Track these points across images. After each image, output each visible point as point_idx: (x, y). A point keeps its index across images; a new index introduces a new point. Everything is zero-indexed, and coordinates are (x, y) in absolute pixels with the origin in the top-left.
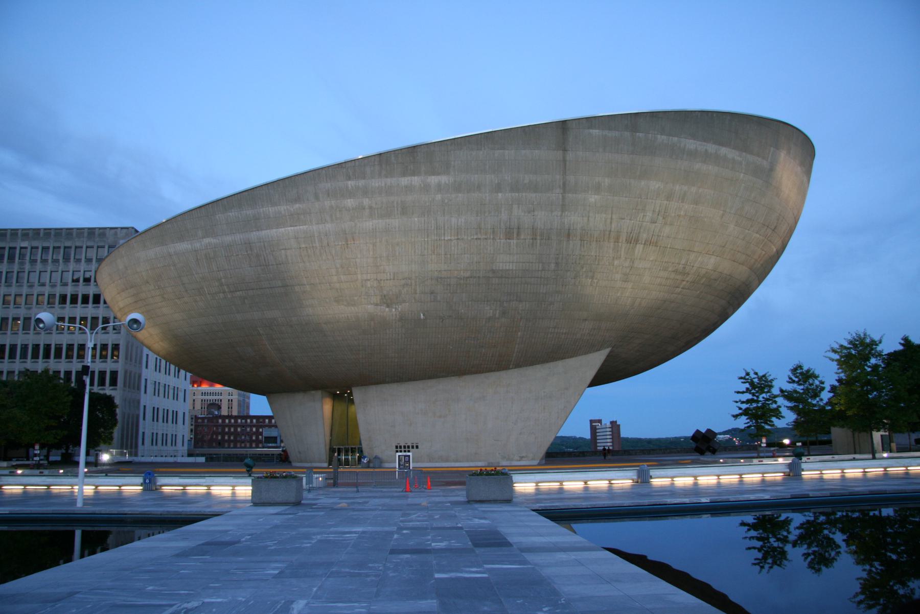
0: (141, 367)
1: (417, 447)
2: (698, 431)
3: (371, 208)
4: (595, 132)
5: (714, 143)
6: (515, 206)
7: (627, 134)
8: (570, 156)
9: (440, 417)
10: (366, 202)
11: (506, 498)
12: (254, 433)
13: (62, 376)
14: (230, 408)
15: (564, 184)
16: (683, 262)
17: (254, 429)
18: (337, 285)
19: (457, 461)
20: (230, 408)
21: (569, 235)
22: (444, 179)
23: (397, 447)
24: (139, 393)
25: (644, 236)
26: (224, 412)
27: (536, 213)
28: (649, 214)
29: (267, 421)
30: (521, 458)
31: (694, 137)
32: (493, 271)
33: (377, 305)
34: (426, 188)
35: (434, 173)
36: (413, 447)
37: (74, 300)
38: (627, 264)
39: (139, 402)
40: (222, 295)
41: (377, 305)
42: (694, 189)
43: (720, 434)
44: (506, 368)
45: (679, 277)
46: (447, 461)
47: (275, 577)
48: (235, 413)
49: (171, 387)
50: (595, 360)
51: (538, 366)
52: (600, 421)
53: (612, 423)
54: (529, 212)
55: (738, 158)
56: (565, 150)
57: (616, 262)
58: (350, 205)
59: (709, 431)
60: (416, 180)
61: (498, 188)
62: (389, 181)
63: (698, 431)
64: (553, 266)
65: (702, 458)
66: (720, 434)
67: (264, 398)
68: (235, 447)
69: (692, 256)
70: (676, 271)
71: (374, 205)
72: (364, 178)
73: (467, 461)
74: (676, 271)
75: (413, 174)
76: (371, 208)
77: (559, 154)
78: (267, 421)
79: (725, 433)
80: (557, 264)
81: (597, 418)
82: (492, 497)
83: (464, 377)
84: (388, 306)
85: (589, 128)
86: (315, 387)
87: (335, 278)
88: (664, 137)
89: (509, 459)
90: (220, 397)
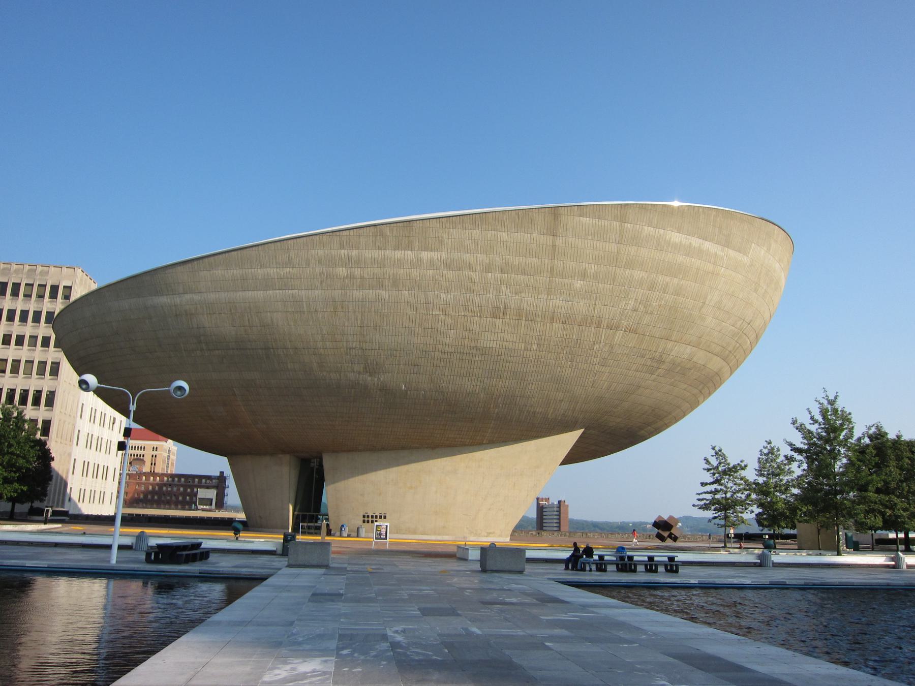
0: (75, 418)
1: (385, 517)
2: (53, 459)
3: (362, 278)
4: (585, 220)
7: (616, 224)
8: (560, 241)
9: (411, 488)
10: (358, 272)
11: (518, 569)
12: (181, 494)
13: (40, 425)
14: (153, 464)
15: (552, 269)
16: (660, 350)
17: (182, 489)
18: (322, 352)
19: (424, 533)
20: (153, 464)
21: (552, 318)
22: (436, 255)
23: (364, 516)
24: (71, 445)
26: (146, 469)
27: (523, 294)
28: (632, 303)
29: (176, 479)
30: (489, 534)
31: (679, 231)
33: (359, 373)
34: (418, 263)
35: (427, 249)
36: (381, 517)
37: (20, 341)
38: (606, 349)
39: (70, 455)
42: (676, 281)
45: (655, 365)
46: (415, 533)
48: (159, 470)
49: (95, 438)
50: (570, 438)
52: (547, 500)
53: (559, 502)
55: (720, 253)
58: (341, 273)
59: (671, 517)
60: (409, 255)
61: (488, 268)
62: (382, 252)
63: (53, 459)
69: (670, 345)
71: (366, 276)
72: (358, 248)
73: (435, 534)
74: (652, 359)
75: (407, 248)
77: (549, 239)
78: (176, 479)
81: (544, 497)
82: (507, 568)
84: (371, 375)
86: (284, 452)
87: (320, 345)
89: (476, 535)
90: (142, 452)
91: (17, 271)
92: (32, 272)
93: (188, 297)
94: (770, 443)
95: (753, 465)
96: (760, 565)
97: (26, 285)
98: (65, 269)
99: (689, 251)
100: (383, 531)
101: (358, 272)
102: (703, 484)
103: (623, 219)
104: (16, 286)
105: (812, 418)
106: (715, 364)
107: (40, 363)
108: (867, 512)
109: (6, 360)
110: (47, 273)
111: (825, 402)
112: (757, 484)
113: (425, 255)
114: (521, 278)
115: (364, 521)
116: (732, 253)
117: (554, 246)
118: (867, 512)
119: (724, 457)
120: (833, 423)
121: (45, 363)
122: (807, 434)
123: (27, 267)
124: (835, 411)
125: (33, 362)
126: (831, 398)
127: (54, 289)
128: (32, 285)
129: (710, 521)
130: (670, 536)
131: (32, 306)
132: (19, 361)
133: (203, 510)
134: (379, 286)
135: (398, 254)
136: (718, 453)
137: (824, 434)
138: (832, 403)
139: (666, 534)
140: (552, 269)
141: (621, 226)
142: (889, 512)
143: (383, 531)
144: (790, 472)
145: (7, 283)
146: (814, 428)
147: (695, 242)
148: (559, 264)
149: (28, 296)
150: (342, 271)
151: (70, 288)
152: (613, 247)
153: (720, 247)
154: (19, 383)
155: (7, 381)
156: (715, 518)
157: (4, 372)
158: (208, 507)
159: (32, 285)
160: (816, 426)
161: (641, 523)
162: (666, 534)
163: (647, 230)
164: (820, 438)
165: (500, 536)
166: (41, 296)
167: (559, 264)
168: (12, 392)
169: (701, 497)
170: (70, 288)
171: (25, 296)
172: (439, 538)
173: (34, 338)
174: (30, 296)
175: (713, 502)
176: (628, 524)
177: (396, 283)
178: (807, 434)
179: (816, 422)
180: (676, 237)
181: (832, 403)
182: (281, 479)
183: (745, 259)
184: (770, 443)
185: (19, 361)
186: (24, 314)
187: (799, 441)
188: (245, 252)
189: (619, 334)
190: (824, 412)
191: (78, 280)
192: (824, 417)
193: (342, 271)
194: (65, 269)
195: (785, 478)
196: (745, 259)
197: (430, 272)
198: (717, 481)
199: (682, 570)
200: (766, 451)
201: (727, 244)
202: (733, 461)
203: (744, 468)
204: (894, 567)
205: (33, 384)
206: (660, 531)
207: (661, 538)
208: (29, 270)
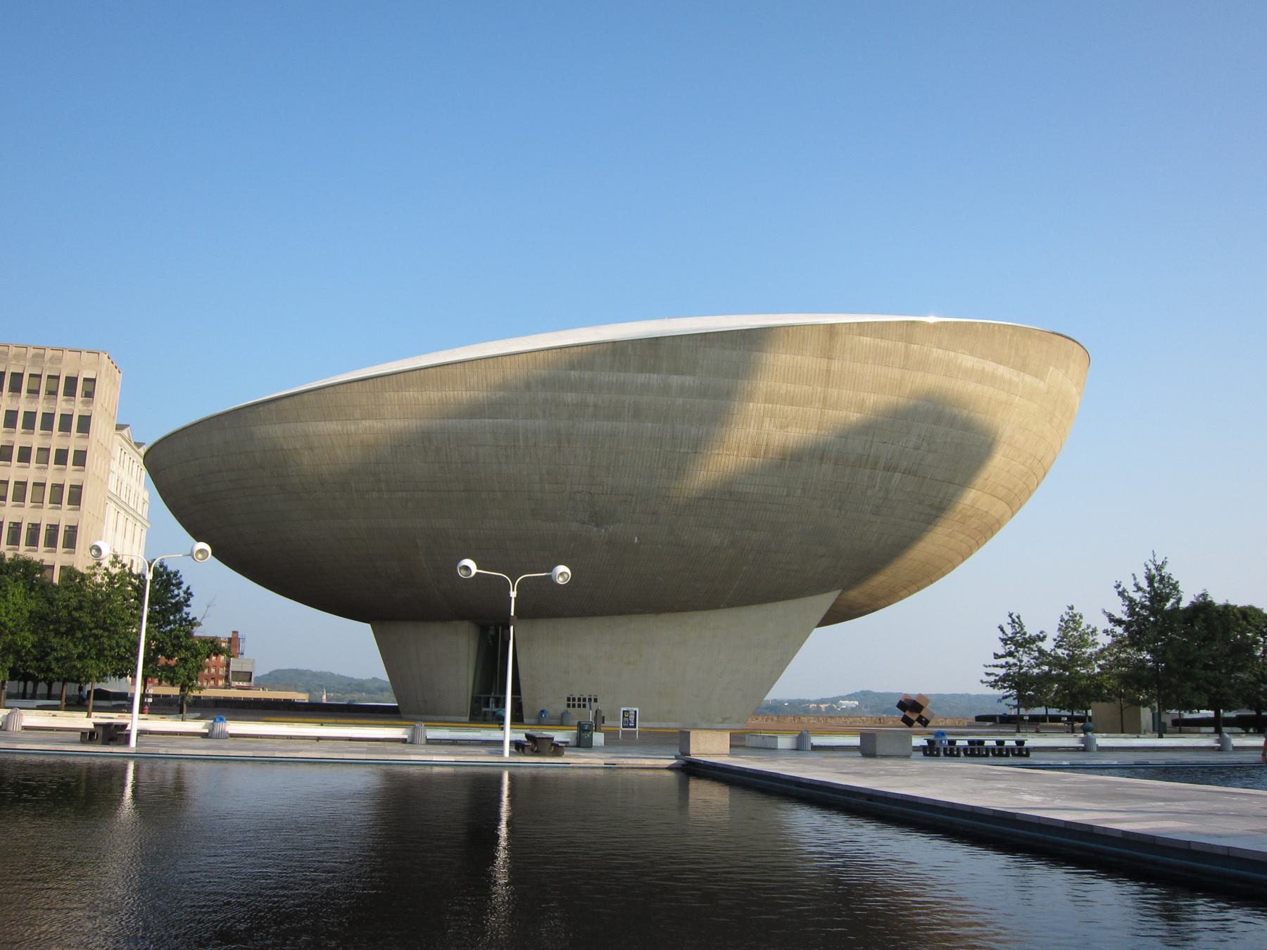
1: (596, 700)
3: (595, 406)
4: (866, 340)
5: (993, 361)
6: (767, 420)
7: (901, 345)
8: (836, 365)
10: (591, 398)
15: (825, 398)
21: (822, 459)
22: (688, 380)
23: (569, 699)
25: (904, 464)
31: (972, 352)
32: (730, 493)
35: (677, 371)
40: (375, 494)
41: (584, 523)
43: (844, 698)
44: (717, 607)
47: (923, 749)
50: (825, 601)
51: (754, 607)
54: (781, 428)
55: (1015, 379)
56: (830, 358)
57: (869, 492)
60: (655, 378)
62: (622, 376)
64: (799, 492)
65: (534, 771)
66: (844, 698)
67: (368, 626)
68: (228, 686)
70: (931, 506)
72: (592, 369)
74: (931, 506)
75: (652, 371)
76: (595, 406)
79: (850, 697)
80: (804, 490)
83: (662, 616)
84: (597, 525)
85: (860, 335)
86: (462, 618)
88: (940, 351)
91: (17, 356)
92: (39, 358)
93: (367, 423)
94: (1071, 608)
95: (1053, 633)
96: (1084, 750)
97: (31, 375)
98: (84, 355)
99: (982, 377)
100: (632, 719)
101: (591, 398)
102: (997, 656)
103: (909, 340)
104: (17, 378)
105: (1136, 585)
106: (1000, 508)
107: (53, 486)
108: (1195, 690)
109: (7, 482)
110: (60, 360)
111: (1152, 567)
112: (1057, 658)
113: (675, 380)
114: (788, 408)
115: (569, 706)
116: (1028, 379)
117: (828, 371)
118: (1195, 690)
119: (1021, 626)
120: (1160, 587)
121: (62, 486)
122: (1131, 603)
123: (31, 352)
124: (1162, 578)
125: (44, 485)
126: (1159, 563)
127: (71, 382)
128: (40, 376)
129: (999, 701)
130: (920, 719)
131: (40, 406)
132: (25, 484)
133: (239, 688)
134: (1072, 719)
135: (642, 378)
136: (1016, 621)
137: (1168, 605)
138: (1159, 568)
139: (914, 717)
140: (825, 398)
141: (906, 347)
142: (1214, 690)
143: (632, 719)
144: (1095, 644)
145: (22, 375)
146: (1137, 597)
147: (989, 366)
148: (834, 392)
149: (34, 392)
150: (570, 397)
151: (94, 380)
152: (896, 373)
153: (1015, 372)
154: (26, 514)
155: (10, 512)
156: (1006, 697)
157: (4, 498)
158: (245, 684)
159: (40, 376)
160: (1140, 594)
161: (802, 702)
162: (914, 717)
163: (937, 352)
164: (1143, 607)
165: (738, 722)
166: (52, 393)
167: (834, 392)
168: (16, 528)
169: (990, 670)
170: (94, 380)
171: (29, 391)
172: (664, 725)
173: (44, 451)
174: (37, 392)
175: (1004, 679)
176: (782, 702)
177: (637, 413)
178: (1131, 603)
179: (1139, 589)
180: (968, 361)
181: (1159, 568)
182: (454, 653)
183: (1042, 386)
184: (1071, 608)
185: (25, 484)
186: (48, 420)
187: (1120, 611)
188: (446, 369)
189: (897, 476)
190: (1150, 579)
191: (104, 369)
192: (1151, 584)
193: (570, 397)
194: (84, 355)
195: (1089, 650)
196: (1042, 386)
197: (680, 401)
198: (1010, 654)
199: (1032, 754)
200: (1066, 618)
201: (1023, 367)
202: (1031, 631)
203: (1042, 639)
204: (1220, 749)
205: (46, 516)
206: (908, 714)
207: (908, 721)
208: (35, 356)
